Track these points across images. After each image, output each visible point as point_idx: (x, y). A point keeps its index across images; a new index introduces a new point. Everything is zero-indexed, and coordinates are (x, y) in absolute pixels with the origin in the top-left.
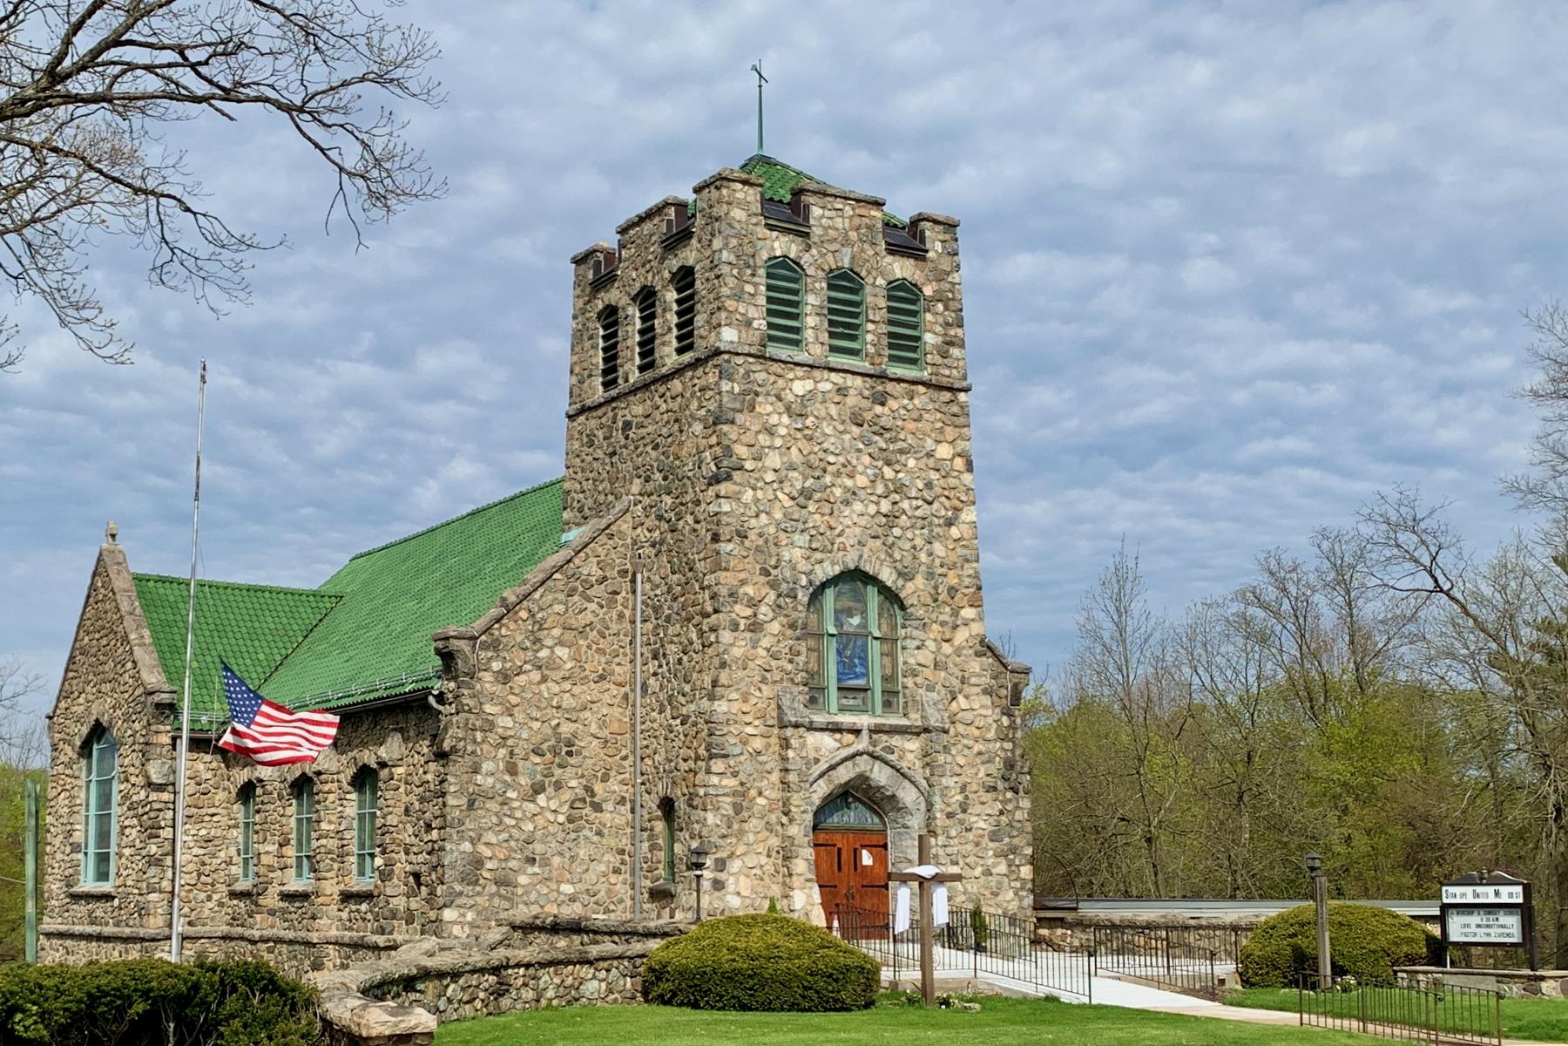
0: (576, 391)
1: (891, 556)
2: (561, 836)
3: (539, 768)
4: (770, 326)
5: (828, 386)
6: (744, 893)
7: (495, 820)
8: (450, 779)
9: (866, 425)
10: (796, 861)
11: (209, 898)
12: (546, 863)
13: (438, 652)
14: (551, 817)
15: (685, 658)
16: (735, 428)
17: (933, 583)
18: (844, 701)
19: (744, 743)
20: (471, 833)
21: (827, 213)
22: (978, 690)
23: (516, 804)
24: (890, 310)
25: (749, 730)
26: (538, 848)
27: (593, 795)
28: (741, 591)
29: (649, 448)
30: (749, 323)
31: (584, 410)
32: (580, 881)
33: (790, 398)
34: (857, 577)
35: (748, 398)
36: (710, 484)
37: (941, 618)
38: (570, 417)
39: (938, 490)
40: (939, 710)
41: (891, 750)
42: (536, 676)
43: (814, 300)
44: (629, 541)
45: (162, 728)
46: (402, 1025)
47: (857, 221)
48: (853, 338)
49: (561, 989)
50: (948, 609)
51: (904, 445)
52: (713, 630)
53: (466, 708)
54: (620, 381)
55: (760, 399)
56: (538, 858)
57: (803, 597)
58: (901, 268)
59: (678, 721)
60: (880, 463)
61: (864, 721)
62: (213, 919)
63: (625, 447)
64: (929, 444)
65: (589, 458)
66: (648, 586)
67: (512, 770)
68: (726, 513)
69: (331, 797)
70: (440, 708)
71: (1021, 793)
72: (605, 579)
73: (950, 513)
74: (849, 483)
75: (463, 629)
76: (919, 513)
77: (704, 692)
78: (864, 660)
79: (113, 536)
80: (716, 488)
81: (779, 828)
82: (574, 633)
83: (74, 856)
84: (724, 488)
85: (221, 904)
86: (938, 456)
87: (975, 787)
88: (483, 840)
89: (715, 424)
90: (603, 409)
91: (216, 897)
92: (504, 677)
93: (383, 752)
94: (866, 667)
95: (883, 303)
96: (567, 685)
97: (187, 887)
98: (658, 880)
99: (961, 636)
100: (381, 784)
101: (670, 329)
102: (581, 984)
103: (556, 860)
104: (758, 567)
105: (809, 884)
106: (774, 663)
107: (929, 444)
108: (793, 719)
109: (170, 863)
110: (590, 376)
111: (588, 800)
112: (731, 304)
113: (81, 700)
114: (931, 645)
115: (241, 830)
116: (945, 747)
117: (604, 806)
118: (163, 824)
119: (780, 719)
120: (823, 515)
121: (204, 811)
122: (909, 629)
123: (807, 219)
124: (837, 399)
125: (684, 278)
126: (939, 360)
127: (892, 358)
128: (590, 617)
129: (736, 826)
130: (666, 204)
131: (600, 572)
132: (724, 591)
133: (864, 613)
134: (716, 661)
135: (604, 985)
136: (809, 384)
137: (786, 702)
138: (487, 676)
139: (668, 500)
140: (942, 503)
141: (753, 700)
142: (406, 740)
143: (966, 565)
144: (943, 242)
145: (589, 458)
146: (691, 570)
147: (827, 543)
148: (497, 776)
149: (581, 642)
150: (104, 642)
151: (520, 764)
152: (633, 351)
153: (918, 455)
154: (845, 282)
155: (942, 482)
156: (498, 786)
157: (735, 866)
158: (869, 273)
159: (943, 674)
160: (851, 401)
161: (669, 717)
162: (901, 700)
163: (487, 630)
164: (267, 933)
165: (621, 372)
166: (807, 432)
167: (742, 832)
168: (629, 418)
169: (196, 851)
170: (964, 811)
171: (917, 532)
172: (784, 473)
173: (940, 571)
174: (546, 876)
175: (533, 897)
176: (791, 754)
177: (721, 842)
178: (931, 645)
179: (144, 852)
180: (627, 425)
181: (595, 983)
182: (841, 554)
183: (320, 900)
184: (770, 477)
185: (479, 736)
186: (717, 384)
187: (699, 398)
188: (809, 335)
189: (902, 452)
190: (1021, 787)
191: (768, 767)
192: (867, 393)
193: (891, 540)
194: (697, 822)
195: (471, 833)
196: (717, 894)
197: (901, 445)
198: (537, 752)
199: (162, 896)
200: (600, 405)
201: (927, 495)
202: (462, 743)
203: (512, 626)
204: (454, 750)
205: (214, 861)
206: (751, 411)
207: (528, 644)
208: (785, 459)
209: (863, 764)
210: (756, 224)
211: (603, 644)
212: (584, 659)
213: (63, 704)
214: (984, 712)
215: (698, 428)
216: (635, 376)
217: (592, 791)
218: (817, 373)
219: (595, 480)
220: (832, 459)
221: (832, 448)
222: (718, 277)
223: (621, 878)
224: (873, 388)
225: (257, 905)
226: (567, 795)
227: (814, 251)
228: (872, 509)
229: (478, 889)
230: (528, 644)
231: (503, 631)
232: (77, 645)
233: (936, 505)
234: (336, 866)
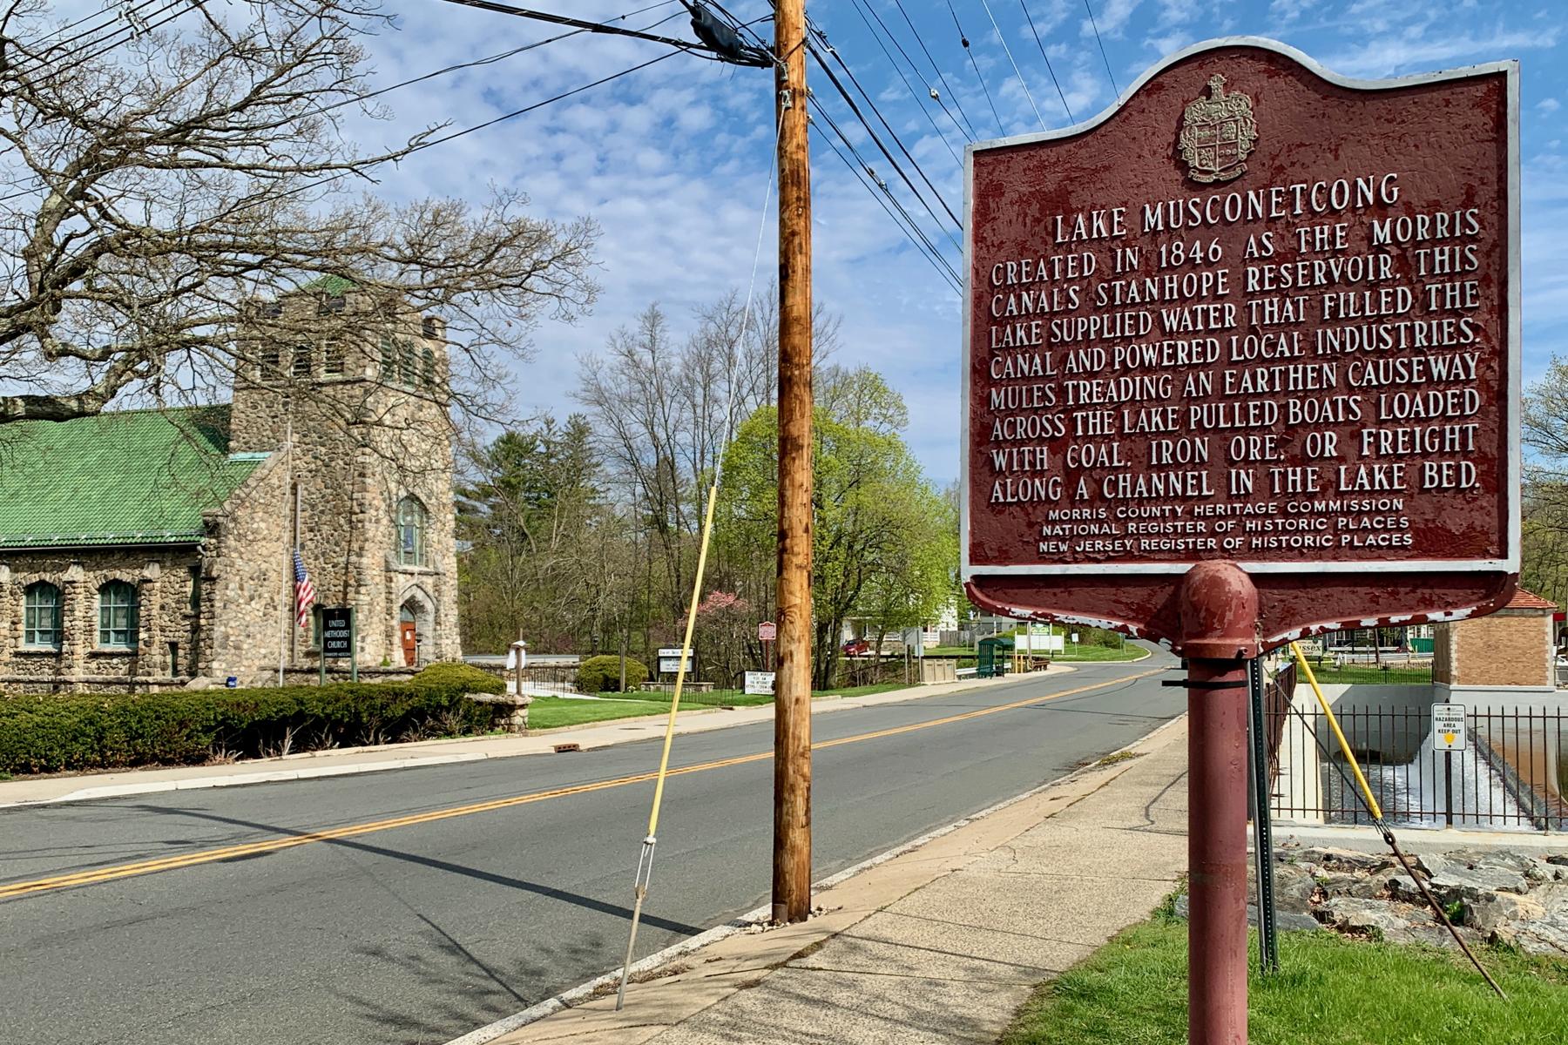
12: (254, 638)
26: (251, 629)
61: (416, 569)
66: (305, 493)
67: (242, 589)
69: (81, 597)
93: (147, 573)
103: (259, 636)
132: (367, 503)
142: (162, 568)
157: (368, 640)
198: (252, 579)
204: (219, 576)
226: (264, 602)
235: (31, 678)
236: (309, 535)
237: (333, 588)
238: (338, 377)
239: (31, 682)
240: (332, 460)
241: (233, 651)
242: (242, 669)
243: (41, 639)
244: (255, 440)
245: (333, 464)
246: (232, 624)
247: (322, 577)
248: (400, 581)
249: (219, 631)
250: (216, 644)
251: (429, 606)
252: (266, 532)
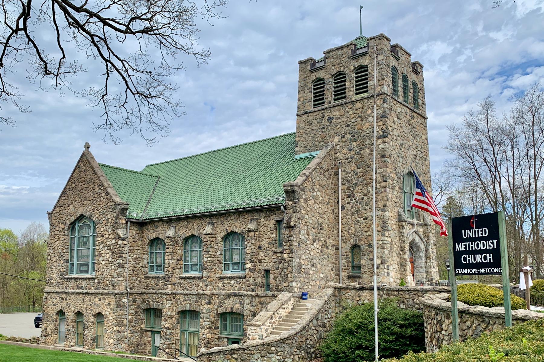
11: (137, 279)
12: (316, 267)
23: (309, 246)
26: (314, 261)
45: (123, 217)
62: (138, 287)
67: (308, 234)
85: (140, 282)
90: (317, 113)
92: (306, 201)
103: (319, 266)
115: (149, 255)
118: (124, 252)
121: (135, 248)
157: (391, 268)
161: (357, 217)
195: (299, 255)
196: (388, 277)
205: (138, 266)
213: (57, 209)
226: (321, 244)
231: (306, 185)
232: (68, 187)
235: (187, 292)
236: (347, 200)
237: (364, 234)
238: (365, 95)
239: (187, 294)
240: (362, 149)
241: (304, 275)
242: (310, 287)
243: (192, 269)
244: (310, 144)
245: (362, 152)
246: (303, 257)
247: (357, 227)
248: (408, 230)
249: (295, 262)
250: (294, 270)
251: (422, 247)
252: (321, 198)
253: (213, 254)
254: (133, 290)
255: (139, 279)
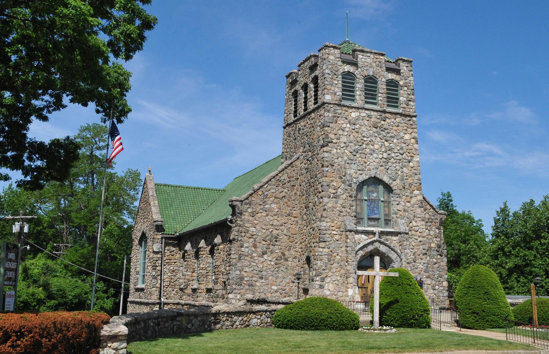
0: (286, 119)
1: (387, 172)
2: (272, 269)
3: (265, 246)
4: (343, 94)
5: (365, 115)
6: (331, 290)
7: (248, 264)
8: (233, 249)
9: (378, 128)
10: (350, 278)
11: (173, 290)
12: (266, 279)
13: (230, 205)
14: (269, 263)
15: (314, 208)
16: (330, 128)
17: (403, 182)
18: (370, 223)
19: (332, 237)
20: (239, 268)
21: (364, 57)
22: (420, 219)
23: (256, 258)
24: (388, 89)
25: (334, 232)
26: (264, 273)
27: (284, 255)
28: (331, 184)
29: (305, 137)
30: (335, 94)
31: (288, 125)
32: (279, 285)
33: (350, 118)
34: (375, 181)
35: (335, 118)
36: (321, 148)
37: (406, 194)
38: (284, 128)
39: (405, 150)
40: (404, 226)
41: (387, 240)
42: (264, 214)
43: (359, 85)
44: (299, 168)
46: (113, 332)
47: (375, 60)
48: (375, 99)
49: (242, 321)
50: (409, 191)
51: (393, 135)
52: (322, 198)
53: (239, 225)
54: (298, 115)
55: (339, 119)
56: (264, 277)
57: (354, 187)
58: (391, 76)
59: (312, 230)
60: (383, 141)
63: (299, 136)
64: (402, 134)
65: (289, 141)
68: (326, 157)
70: (231, 225)
71: (443, 256)
72: (290, 181)
73: (409, 158)
74: (372, 147)
75: (238, 198)
76: (397, 158)
77: (318, 219)
78: (378, 209)
79: (150, 171)
80: (323, 149)
81: (345, 267)
82: (278, 199)
83: (137, 276)
84: (325, 149)
86: (405, 139)
87: (418, 253)
88: (244, 270)
89: (323, 127)
91: (175, 290)
92: (253, 215)
94: (379, 211)
95: (384, 87)
96: (276, 217)
97: (166, 286)
98: (306, 285)
99: (414, 200)
100: (215, 251)
101: (312, 97)
102: (250, 320)
104: (338, 176)
105: (354, 287)
106: (343, 209)
107: (402, 134)
108: (350, 229)
109: (160, 278)
110: (290, 114)
111: (283, 257)
112: (328, 87)
113: (140, 225)
114: (403, 203)
116: (406, 239)
117: (289, 259)
118: (157, 265)
119: (345, 229)
120: (362, 158)
122: (394, 198)
123: (357, 59)
124: (368, 119)
125: (315, 80)
126: (405, 106)
127: (388, 106)
128: (284, 194)
129: (328, 266)
130: (311, 56)
131: (288, 179)
133: (378, 192)
134: (322, 209)
135: (259, 320)
136: (357, 114)
137: (347, 223)
138: (247, 214)
139: (310, 153)
140: (406, 154)
141: (336, 222)
143: (416, 176)
144: (407, 67)
145: (289, 141)
146: (316, 177)
147: (363, 168)
148: (249, 248)
149: (281, 203)
150: (145, 205)
151: (258, 244)
152: (302, 104)
153: (398, 138)
154: (371, 81)
155: (407, 147)
156: (250, 252)
157: (328, 280)
158: (379, 77)
159: (407, 213)
160: (373, 120)
162: (392, 223)
163: (247, 199)
164: (187, 302)
165: (298, 112)
166: (356, 130)
167: (331, 268)
168: (300, 127)
169: (169, 274)
170: (415, 262)
171: (397, 164)
172: (347, 144)
173: (406, 178)
174: (267, 283)
175: (262, 290)
176: (348, 241)
177: (323, 272)
178: (403, 203)
179: (152, 274)
180: (299, 129)
181: (256, 320)
182: (369, 172)
183: (199, 291)
184: (343, 145)
185: (243, 234)
186: (324, 114)
187: (319, 119)
188: (357, 97)
189: (391, 137)
190: (443, 254)
191: (341, 246)
192: (378, 117)
193: (387, 167)
194: (315, 264)
195: (239, 268)
197: (391, 135)
199: (157, 289)
200: (292, 123)
201: (401, 152)
202: (237, 237)
203: (256, 196)
204: (234, 239)
206: (336, 123)
207: (261, 203)
208: (348, 139)
209: (377, 245)
210: (338, 61)
211: (289, 203)
212: (282, 208)
214: (422, 227)
215: (319, 128)
216: (302, 113)
217: (284, 254)
218: (360, 110)
219: (290, 148)
220: (365, 139)
221: (366, 135)
222: (324, 78)
223: (294, 284)
224: (381, 115)
225: (184, 293)
226: (275, 255)
227: (359, 70)
228: (380, 156)
229: (242, 287)
230: (261, 203)
231: (253, 199)
233: (404, 155)
234: (205, 279)
253: (204, 266)
254: (169, 300)
255: (175, 290)
